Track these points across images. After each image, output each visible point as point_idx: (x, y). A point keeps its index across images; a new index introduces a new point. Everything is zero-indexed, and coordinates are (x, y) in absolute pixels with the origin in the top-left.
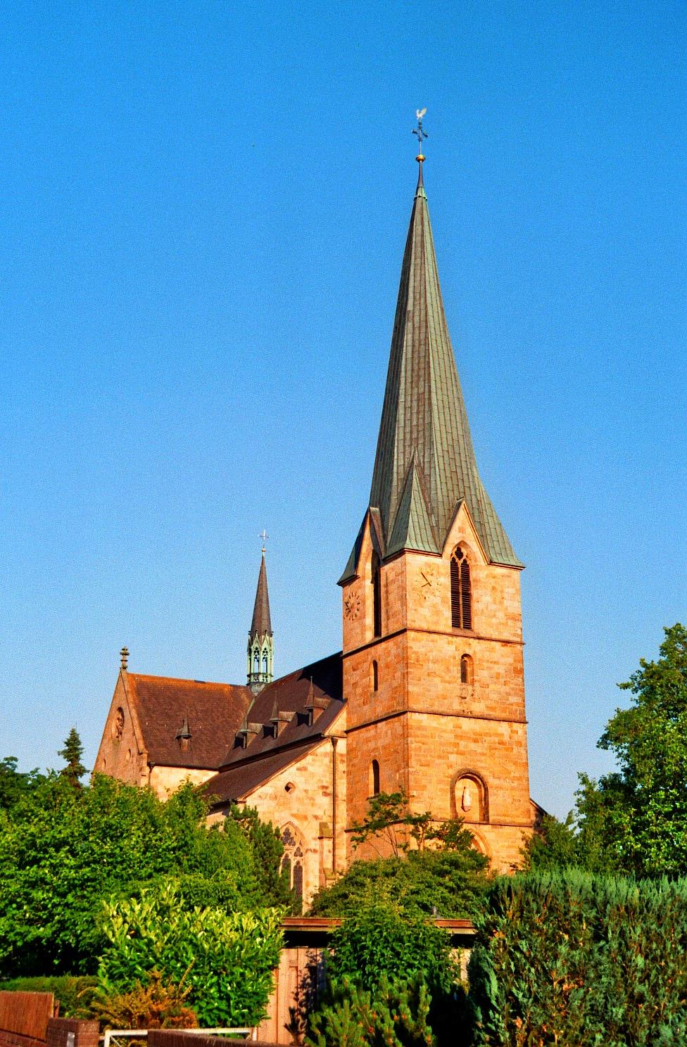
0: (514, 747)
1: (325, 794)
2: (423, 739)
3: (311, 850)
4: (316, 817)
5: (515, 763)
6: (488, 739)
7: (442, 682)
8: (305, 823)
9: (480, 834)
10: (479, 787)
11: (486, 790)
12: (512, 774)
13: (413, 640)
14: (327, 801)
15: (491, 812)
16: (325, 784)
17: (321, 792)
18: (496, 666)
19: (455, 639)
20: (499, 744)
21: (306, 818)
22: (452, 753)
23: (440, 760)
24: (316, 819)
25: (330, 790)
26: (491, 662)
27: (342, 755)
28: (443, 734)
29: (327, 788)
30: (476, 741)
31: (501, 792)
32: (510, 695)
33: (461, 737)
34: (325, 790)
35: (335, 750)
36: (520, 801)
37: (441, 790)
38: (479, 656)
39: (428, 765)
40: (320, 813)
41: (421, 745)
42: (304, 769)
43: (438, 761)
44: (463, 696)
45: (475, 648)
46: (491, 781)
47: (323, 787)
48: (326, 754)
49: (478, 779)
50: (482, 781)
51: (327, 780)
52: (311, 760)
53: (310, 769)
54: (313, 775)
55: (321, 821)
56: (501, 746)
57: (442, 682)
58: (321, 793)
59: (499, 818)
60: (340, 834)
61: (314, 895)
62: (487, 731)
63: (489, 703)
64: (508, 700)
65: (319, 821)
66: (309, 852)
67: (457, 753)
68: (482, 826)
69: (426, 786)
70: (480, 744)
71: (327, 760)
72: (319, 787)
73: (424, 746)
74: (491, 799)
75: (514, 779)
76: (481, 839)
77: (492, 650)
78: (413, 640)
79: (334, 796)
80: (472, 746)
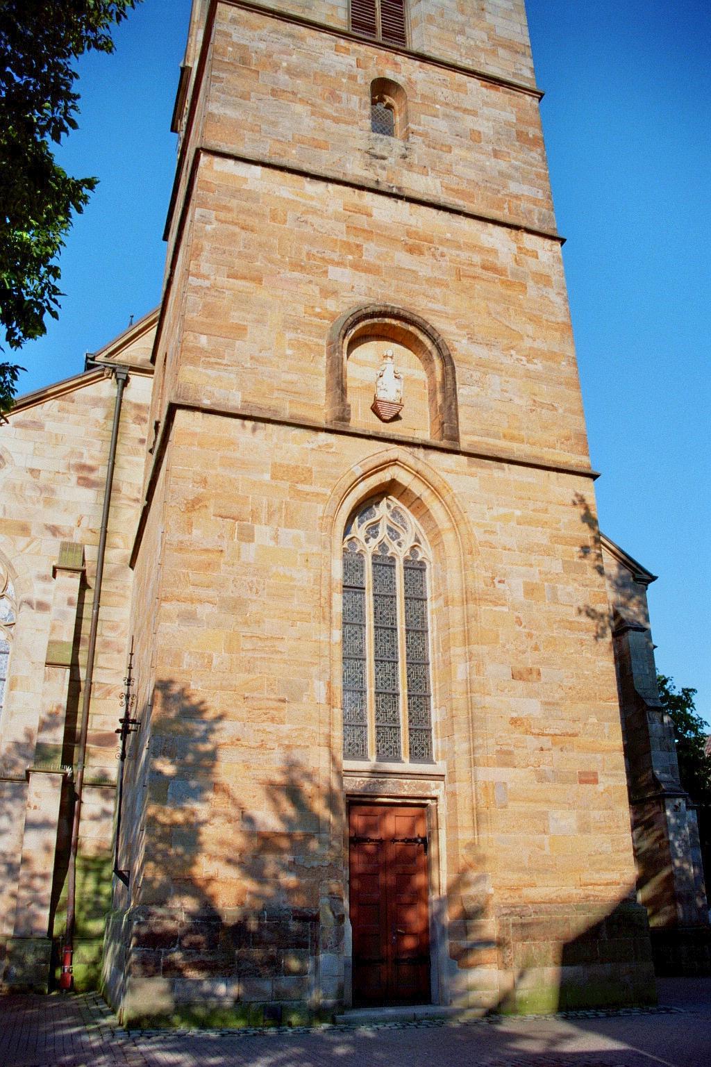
0: (530, 283)
1: (86, 483)
2: (242, 217)
3: (29, 603)
4: (54, 530)
5: (534, 319)
6: (451, 252)
7: (313, 114)
8: (22, 541)
9: (430, 475)
10: (428, 360)
11: (447, 361)
12: (528, 343)
13: (234, 21)
14: (90, 498)
15: (464, 424)
16: (89, 462)
17: (74, 477)
18: (469, 118)
19: (354, 46)
20: (484, 268)
21: (24, 529)
22: (338, 264)
23: (296, 274)
24: (54, 535)
25: (101, 474)
26: (456, 108)
27: (139, 407)
28: (310, 218)
29: (91, 469)
30: (411, 250)
31: (495, 380)
32: (510, 177)
33: (368, 234)
34: (85, 474)
35: (121, 394)
36: (555, 409)
37: (298, 345)
38: (419, 88)
39: (258, 280)
40: (65, 521)
41: (237, 230)
42: (37, 425)
43: (287, 274)
44: (378, 151)
45: (402, 70)
46: (461, 346)
47: (83, 467)
48: (96, 402)
49: (422, 337)
50: (434, 341)
51: (96, 454)
52: (56, 410)
53: (50, 426)
54: (57, 439)
55: (67, 540)
56: (490, 274)
57: (313, 114)
58: (74, 478)
59: (491, 441)
60: (115, 573)
61: (468, 844)
62: (448, 235)
63: (453, 182)
64: (505, 187)
65: (61, 539)
66: (25, 608)
67: (355, 266)
68: (435, 456)
69: (244, 328)
70: (427, 258)
71: (99, 414)
72: (69, 467)
73: (243, 234)
74: (464, 393)
75: (532, 355)
76: (436, 491)
77: (460, 87)
78: (234, 21)
79: (110, 488)
80: (404, 259)
